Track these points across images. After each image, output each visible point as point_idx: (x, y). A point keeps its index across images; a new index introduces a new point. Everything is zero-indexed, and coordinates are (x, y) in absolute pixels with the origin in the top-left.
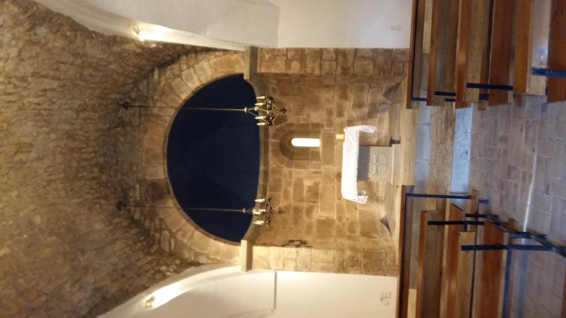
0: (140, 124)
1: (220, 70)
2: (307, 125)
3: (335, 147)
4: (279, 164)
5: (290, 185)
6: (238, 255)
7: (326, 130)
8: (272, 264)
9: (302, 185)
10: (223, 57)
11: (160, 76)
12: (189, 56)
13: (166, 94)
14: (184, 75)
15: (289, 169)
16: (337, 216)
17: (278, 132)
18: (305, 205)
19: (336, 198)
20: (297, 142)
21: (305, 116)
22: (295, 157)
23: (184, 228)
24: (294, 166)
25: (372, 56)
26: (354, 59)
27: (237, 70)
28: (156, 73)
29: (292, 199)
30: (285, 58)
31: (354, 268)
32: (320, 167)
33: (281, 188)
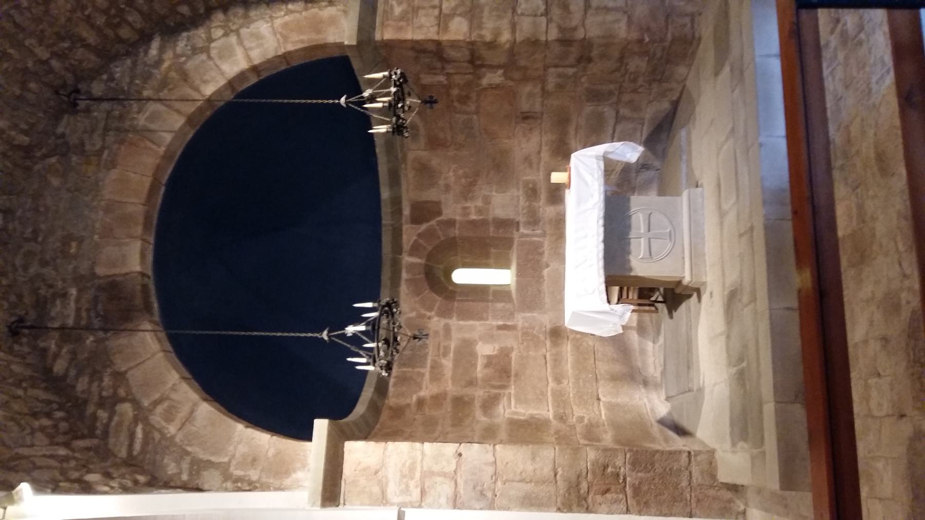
0: (103, 148)
1: (295, 37)
2: (484, 223)
3: (545, 272)
4: (423, 311)
5: (445, 355)
6: (304, 466)
7: (523, 235)
8: (392, 489)
9: (473, 355)
10: (304, 13)
11: (162, 50)
12: (230, 13)
13: (170, 87)
14: (214, 48)
15: (443, 322)
16: (554, 412)
17: (421, 241)
18: (479, 393)
19: (550, 379)
20: (462, 276)
21: (479, 203)
22: (458, 298)
23: (174, 396)
24: (455, 315)
25: (623, 5)
26: (586, 12)
27: (332, 36)
28: (155, 44)
29: (450, 382)
30: (436, 12)
31: (608, 496)
32: (512, 314)
33: (426, 359)
